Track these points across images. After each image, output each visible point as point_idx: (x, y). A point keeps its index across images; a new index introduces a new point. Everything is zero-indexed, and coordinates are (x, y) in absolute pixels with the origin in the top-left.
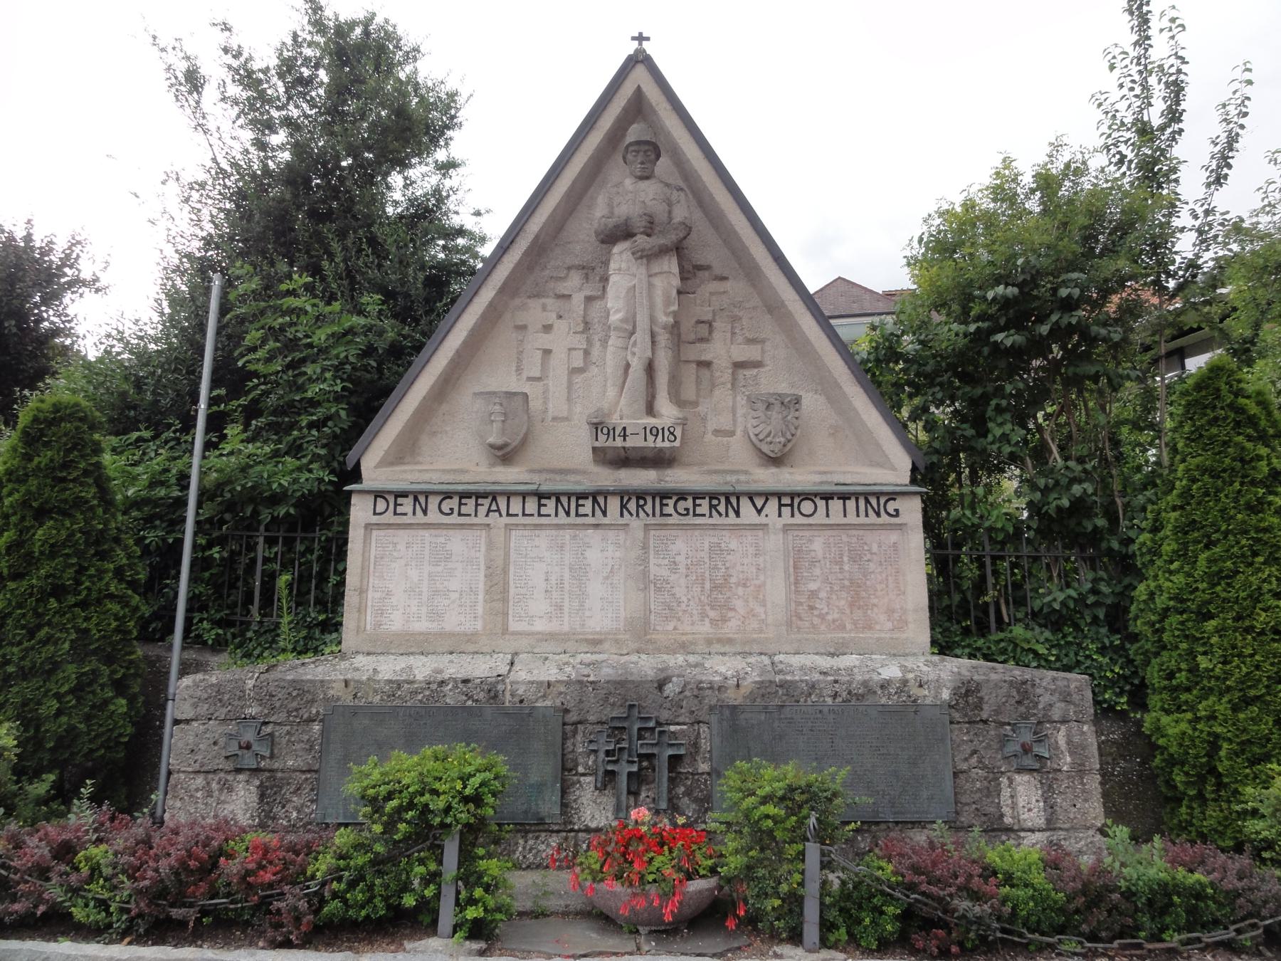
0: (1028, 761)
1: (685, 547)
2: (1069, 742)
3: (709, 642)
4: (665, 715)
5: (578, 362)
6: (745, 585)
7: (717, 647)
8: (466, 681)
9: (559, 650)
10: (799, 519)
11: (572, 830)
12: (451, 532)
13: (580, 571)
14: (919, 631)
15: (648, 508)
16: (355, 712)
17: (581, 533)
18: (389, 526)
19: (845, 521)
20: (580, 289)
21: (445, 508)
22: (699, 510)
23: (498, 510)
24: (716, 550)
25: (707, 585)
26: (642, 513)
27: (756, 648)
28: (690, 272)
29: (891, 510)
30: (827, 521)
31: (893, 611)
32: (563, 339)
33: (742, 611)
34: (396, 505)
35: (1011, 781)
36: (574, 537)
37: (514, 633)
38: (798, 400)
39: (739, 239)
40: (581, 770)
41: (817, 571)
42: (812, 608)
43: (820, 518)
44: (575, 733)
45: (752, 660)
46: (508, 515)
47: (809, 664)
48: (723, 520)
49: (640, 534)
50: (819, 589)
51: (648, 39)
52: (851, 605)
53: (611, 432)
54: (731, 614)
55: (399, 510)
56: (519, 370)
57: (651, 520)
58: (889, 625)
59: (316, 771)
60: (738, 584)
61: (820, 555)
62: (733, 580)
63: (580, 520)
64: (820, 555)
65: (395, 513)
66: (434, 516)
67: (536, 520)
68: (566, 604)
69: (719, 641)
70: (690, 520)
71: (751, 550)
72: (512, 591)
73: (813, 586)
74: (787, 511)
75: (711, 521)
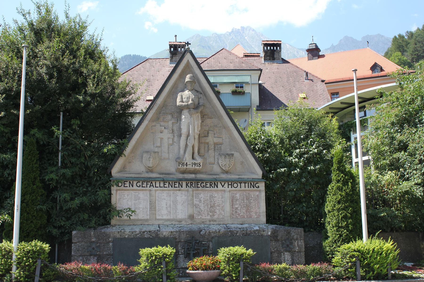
0: (288, 249)
1: (204, 195)
2: (298, 244)
3: (210, 221)
4: (201, 239)
5: (171, 142)
6: (219, 206)
7: (212, 223)
8: (150, 232)
9: (171, 224)
10: (233, 188)
11: (178, 268)
12: (140, 192)
13: (175, 202)
14: (264, 219)
15: (194, 185)
16: (121, 239)
17: (175, 192)
18: (122, 190)
19: (245, 189)
20: (171, 120)
21: (138, 185)
22: (207, 186)
23: (153, 186)
24: (211, 197)
25: (209, 206)
26: (192, 187)
27: (222, 223)
28: (203, 116)
29: (257, 186)
30: (241, 189)
31: (257, 213)
32: (166, 135)
33: (218, 213)
34: (124, 184)
35: (284, 254)
36: (173, 193)
37: (158, 219)
38: (233, 155)
39: (217, 107)
40: (180, 253)
41: (238, 202)
42: (236, 212)
43: (239, 188)
44: (178, 244)
45: (221, 226)
46: (156, 187)
47: (236, 226)
48: (213, 189)
49: (191, 193)
50: (238, 207)
51: (190, 44)
52: (246, 211)
53: (183, 164)
54: (215, 214)
55: (125, 185)
56: (154, 144)
57: (194, 189)
58: (256, 216)
59: (112, 255)
60: (217, 206)
61: (238, 198)
62: (216, 205)
63: (175, 188)
64: (238, 198)
65: (124, 186)
66: (135, 187)
67: (163, 188)
68: (172, 211)
69: (212, 221)
70: (205, 188)
71: (221, 197)
72: (157, 208)
73: (236, 206)
74: (230, 186)
75: (210, 189)
